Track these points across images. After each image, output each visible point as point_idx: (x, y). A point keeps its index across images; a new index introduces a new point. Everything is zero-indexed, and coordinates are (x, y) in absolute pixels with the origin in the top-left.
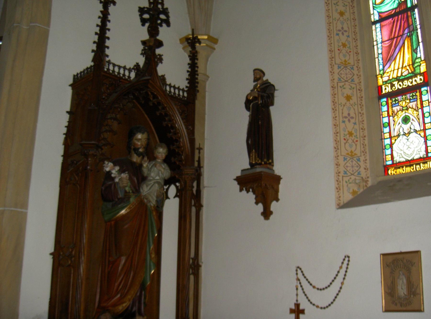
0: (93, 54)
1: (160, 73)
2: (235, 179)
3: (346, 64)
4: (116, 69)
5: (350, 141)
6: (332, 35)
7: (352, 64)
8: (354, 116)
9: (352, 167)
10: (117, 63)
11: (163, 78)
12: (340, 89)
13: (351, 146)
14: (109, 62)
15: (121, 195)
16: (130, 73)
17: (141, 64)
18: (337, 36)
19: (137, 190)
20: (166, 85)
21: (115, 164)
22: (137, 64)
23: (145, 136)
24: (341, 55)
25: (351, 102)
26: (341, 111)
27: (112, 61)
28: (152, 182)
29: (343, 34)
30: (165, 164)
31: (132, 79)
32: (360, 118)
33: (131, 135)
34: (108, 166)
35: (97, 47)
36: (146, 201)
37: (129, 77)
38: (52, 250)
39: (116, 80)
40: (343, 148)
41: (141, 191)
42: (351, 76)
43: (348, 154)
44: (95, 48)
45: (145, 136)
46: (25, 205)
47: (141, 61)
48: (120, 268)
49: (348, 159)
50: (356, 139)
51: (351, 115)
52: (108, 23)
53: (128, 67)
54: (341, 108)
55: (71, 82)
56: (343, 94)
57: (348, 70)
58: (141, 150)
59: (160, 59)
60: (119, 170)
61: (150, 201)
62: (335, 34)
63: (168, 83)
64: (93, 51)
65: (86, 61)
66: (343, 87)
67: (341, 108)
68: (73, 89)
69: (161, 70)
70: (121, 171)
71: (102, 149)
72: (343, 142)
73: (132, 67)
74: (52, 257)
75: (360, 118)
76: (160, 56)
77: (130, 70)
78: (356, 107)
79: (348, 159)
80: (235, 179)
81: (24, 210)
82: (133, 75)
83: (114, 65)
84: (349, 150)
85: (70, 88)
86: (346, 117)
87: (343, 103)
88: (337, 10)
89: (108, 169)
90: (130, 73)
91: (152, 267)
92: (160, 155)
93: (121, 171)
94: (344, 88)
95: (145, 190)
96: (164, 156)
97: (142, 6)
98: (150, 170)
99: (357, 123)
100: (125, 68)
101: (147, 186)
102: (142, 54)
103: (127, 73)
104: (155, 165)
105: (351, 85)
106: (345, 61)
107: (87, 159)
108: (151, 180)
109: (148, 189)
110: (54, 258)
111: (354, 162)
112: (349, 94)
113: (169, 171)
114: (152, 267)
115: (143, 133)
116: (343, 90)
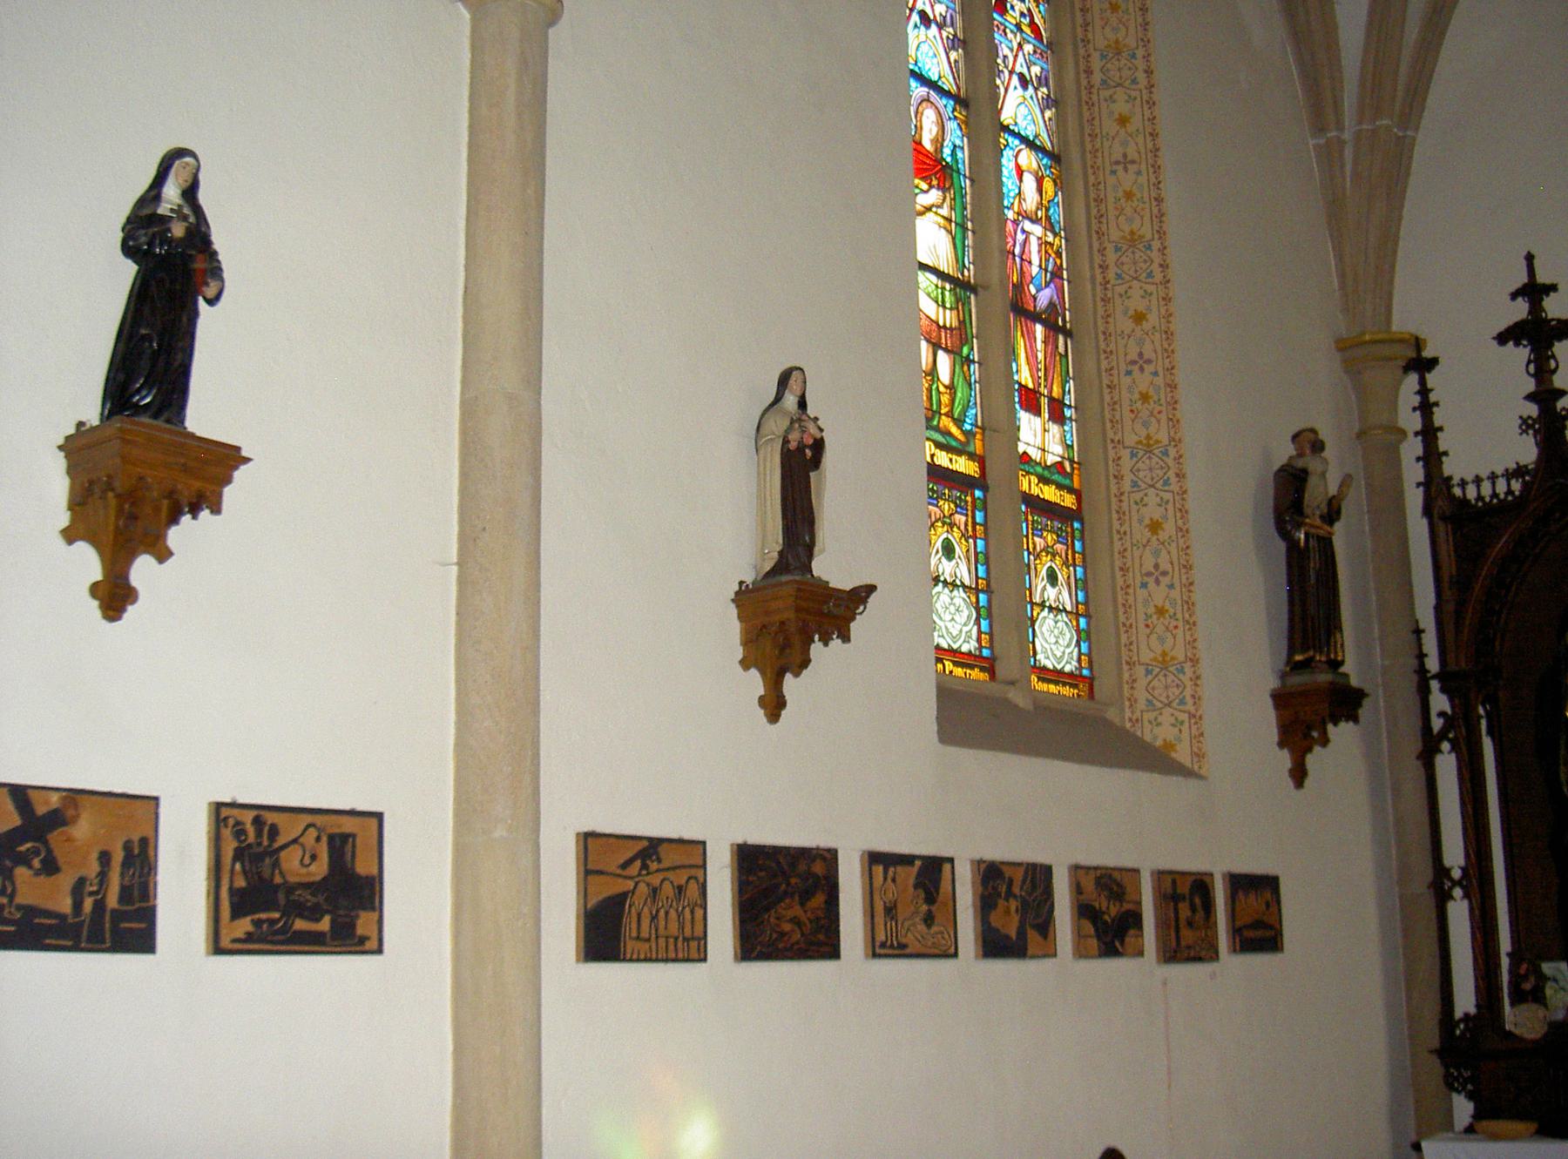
2: (247, 460)
3: (1149, 445)
5: (1160, 629)
6: (1132, 620)
7: (1148, 236)
8: (1168, 567)
9: (1166, 687)
12: (1118, 301)
13: (1162, 640)
17: (788, 677)
18: (1144, 591)
24: (1108, 29)
25: (1145, 325)
26: (1137, 561)
29: (1157, 582)
32: (1181, 541)
40: (1143, 647)
42: (1161, 473)
43: (1140, 442)
49: (1141, 453)
50: (1174, 623)
51: (1162, 568)
54: (1122, 342)
56: (1140, 521)
57: (1170, 678)
62: (1123, 373)
66: (1125, 295)
67: (1137, 554)
72: (1127, 416)
75: (1194, 728)
78: (1140, 140)
79: (1141, 453)
80: (247, 460)
84: (1127, 229)
86: (1149, 574)
87: (1112, 134)
88: (1127, 309)
94: (1159, 724)
99: (1177, 585)
105: (1177, 714)
106: (1132, 233)
111: (1138, 254)
112: (1141, 308)
116: (1112, 106)
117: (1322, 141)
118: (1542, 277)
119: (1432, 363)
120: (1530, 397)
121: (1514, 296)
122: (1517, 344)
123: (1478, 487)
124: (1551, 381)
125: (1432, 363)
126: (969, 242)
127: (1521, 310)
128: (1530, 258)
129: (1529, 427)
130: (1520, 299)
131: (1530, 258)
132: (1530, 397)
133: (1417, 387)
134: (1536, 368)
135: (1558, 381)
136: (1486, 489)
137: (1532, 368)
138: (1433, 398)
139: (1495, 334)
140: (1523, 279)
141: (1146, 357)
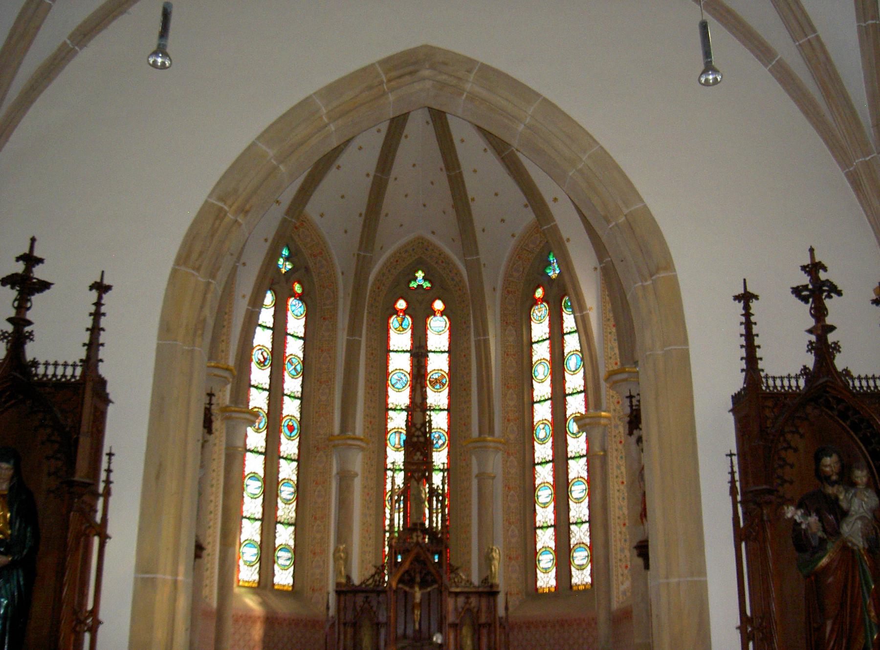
0: (744, 373)
1: (840, 368)
4: (778, 383)
10: (776, 375)
11: (847, 372)
14: (767, 377)
15: (814, 542)
16: (797, 381)
17: (811, 365)
19: (833, 532)
20: (852, 378)
21: (798, 507)
22: (805, 367)
23: (835, 457)
27: (770, 374)
28: (854, 518)
30: (870, 490)
31: (801, 388)
33: (818, 459)
34: (790, 512)
35: (746, 363)
36: (850, 544)
37: (798, 387)
38: (739, 624)
39: (780, 399)
41: (842, 531)
44: (744, 367)
45: (835, 457)
46: (702, 572)
47: (810, 361)
48: (827, 635)
52: (754, 326)
53: (793, 375)
55: (730, 406)
58: (834, 478)
59: (836, 347)
60: (802, 514)
61: (854, 544)
63: (855, 375)
64: (743, 370)
65: (737, 382)
68: (734, 414)
69: (840, 363)
70: (807, 514)
71: (778, 491)
73: (799, 373)
74: (738, 631)
76: (836, 344)
77: (797, 378)
81: (702, 579)
82: (802, 383)
83: (774, 378)
85: (731, 414)
89: (789, 515)
90: (797, 381)
91: (874, 629)
92: (859, 480)
93: (807, 514)
95: (845, 529)
96: (865, 480)
97: (795, 286)
98: (850, 502)
100: (789, 377)
101: (847, 525)
102: (809, 351)
103: (793, 383)
104: (855, 495)
107: (762, 509)
108: (852, 516)
109: (850, 527)
110: (741, 633)
113: (877, 499)
114: (874, 629)
115: (830, 456)
117: (77, 48)
118: (37, 253)
119: (108, 288)
120: (10, 320)
121: (18, 259)
122: (12, 288)
123: (65, 369)
124: (25, 314)
125: (108, 288)
126: (387, 522)
127: (20, 268)
128: (33, 240)
129: (6, 338)
130: (21, 262)
131: (33, 240)
132: (10, 320)
133: (95, 300)
134: (19, 305)
135: (29, 315)
136: (51, 371)
137: (16, 304)
138: (103, 309)
139: (836, 330)
140: (26, 250)
141: (790, 451)
